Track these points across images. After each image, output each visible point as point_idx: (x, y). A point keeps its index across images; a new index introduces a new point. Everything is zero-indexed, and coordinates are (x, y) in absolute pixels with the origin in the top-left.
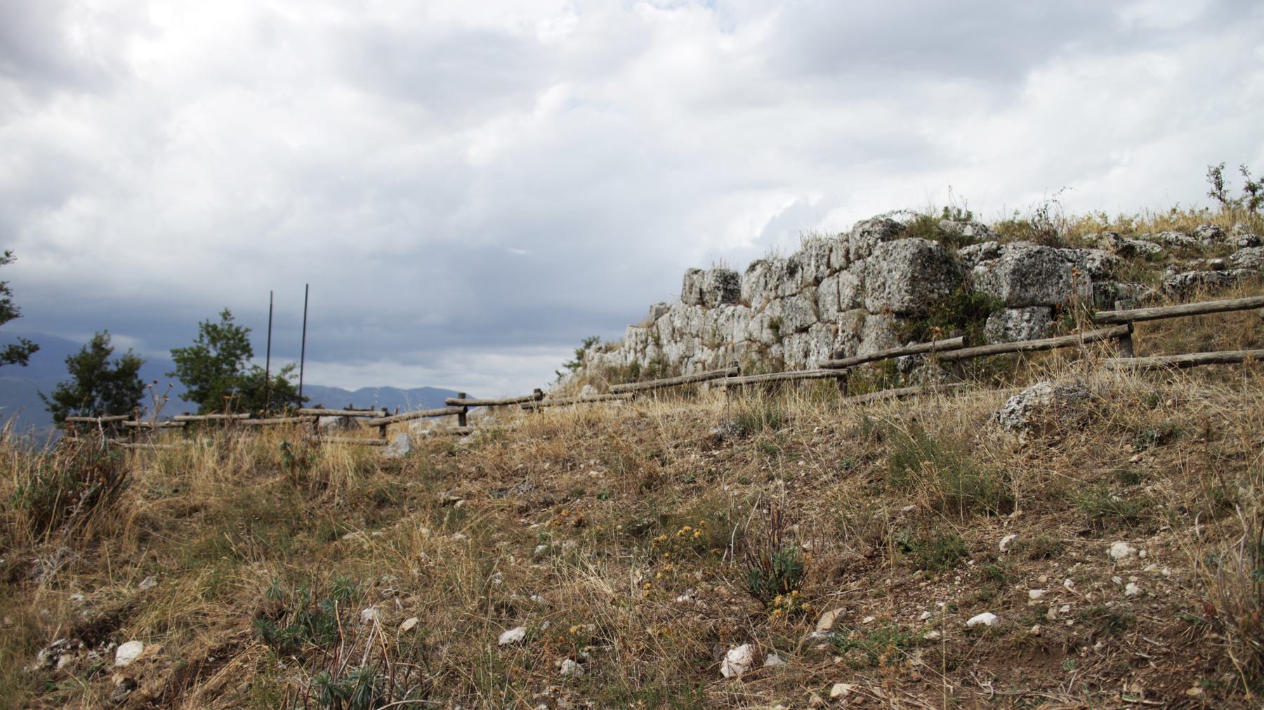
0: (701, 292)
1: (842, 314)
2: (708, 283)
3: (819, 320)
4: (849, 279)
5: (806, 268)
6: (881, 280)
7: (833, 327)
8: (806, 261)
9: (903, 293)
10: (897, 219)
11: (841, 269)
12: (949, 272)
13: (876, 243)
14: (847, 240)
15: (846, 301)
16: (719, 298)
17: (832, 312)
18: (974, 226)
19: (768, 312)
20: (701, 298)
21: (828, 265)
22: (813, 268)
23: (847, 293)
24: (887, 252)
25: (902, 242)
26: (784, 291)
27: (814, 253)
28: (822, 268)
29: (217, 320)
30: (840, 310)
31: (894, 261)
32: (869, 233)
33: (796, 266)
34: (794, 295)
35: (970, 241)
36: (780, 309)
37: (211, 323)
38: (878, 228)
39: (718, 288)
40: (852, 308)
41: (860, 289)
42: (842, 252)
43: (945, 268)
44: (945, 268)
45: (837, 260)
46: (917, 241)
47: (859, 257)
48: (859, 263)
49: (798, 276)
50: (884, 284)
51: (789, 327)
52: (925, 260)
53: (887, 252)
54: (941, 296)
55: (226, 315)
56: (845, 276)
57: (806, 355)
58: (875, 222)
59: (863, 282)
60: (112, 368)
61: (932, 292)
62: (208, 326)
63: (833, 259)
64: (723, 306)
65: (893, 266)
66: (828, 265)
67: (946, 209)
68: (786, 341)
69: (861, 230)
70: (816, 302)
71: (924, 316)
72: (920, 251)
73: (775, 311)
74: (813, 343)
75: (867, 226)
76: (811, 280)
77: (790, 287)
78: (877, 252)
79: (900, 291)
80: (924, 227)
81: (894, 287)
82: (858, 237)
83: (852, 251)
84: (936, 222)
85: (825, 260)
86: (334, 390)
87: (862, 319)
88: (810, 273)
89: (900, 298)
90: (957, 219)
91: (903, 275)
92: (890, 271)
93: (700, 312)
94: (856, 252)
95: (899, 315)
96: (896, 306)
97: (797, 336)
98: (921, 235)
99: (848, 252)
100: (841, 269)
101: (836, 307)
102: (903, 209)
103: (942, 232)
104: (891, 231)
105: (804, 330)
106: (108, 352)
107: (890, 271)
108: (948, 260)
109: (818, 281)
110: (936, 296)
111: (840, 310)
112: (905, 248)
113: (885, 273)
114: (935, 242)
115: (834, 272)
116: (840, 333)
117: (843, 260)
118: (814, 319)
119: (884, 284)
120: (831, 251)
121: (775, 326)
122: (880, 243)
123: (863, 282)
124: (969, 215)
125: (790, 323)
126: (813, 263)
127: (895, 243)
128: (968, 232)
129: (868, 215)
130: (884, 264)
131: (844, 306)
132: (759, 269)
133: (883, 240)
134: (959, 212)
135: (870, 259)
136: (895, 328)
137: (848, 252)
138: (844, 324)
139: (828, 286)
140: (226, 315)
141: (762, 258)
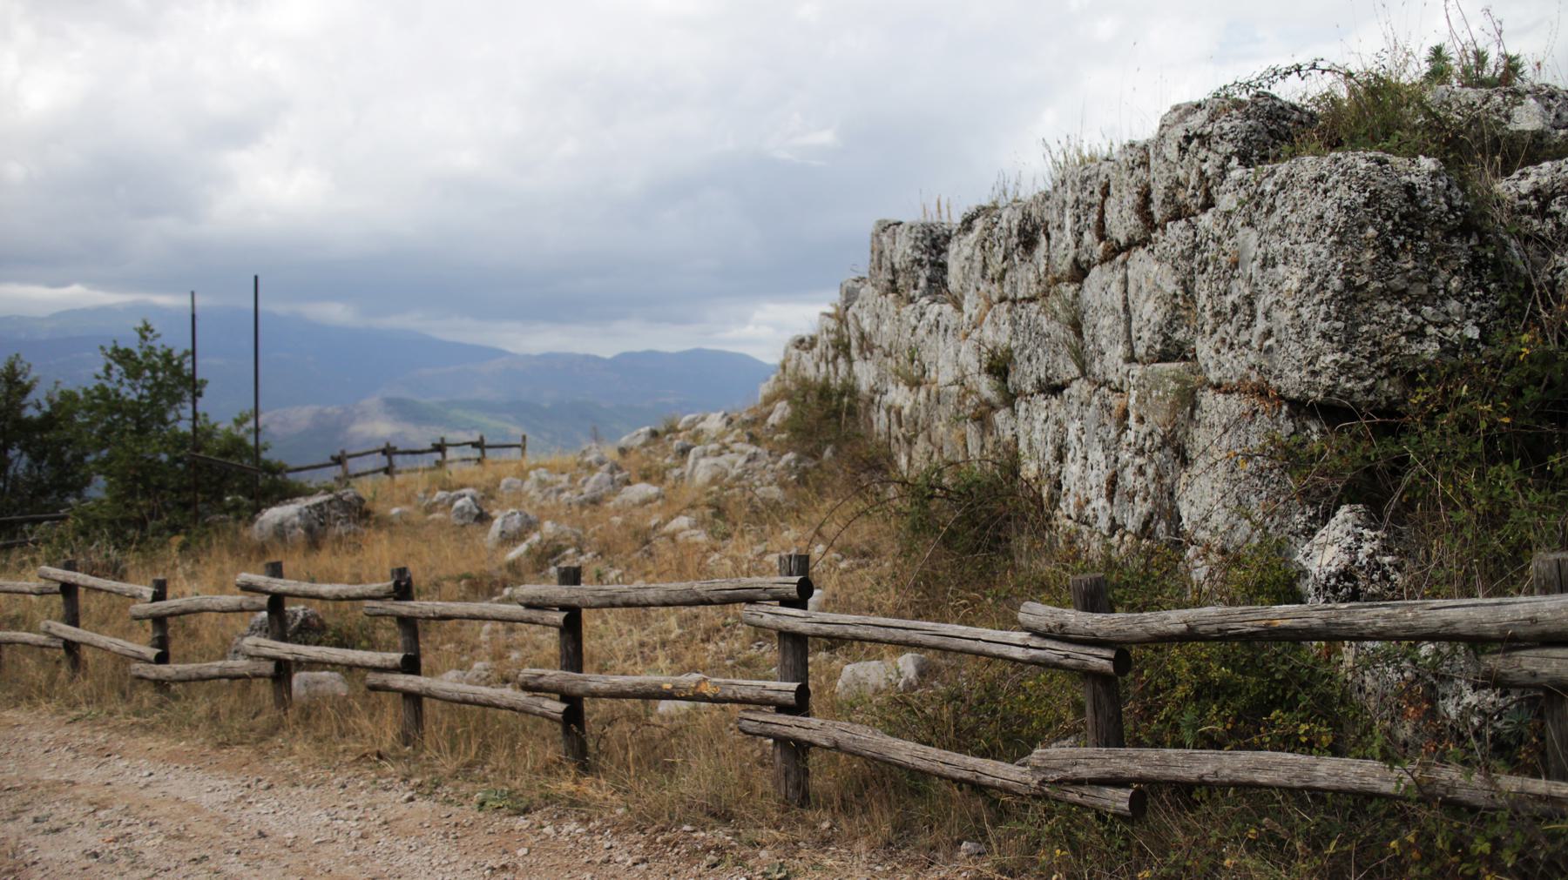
0: (894, 271)
1: (1137, 370)
2: (902, 250)
3: (1084, 374)
4: (1151, 273)
5: (1054, 234)
6: (1240, 289)
7: (1115, 401)
8: (1052, 216)
9: (1314, 341)
10: (1289, 91)
11: (1131, 245)
12: (1476, 265)
13: (1223, 170)
14: (1145, 164)
15: (1146, 338)
16: (922, 283)
17: (1112, 361)
18: (1547, 96)
19: (988, 333)
20: (893, 282)
21: (1102, 235)
22: (1069, 238)
23: (1149, 312)
24: (1256, 199)
25: (1308, 166)
26: (1014, 286)
27: (1070, 198)
28: (1088, 237)
29: (132, 343)
30: (1131, 359)
31: (1280, 230)
32: (1204, 139)
33: (1036, 228)
34: (1032, 299)
35: (1535, 149)
36: (1007, 328)
37: (121, 347)
38: (1233, 123)
39: (919, 262)
40: (1164, 357)
41: (1181, 307)
42: (1131, 199)
43: (1462, 250)
44: (1462, 250)
45: (1121, 223)
46: (1360, 161)
47: (1179, 213)
48: (1176, 229)
49: (1040, 251)
50: (1250, 301)
51: (1026, 375)
52: (1400, 222)
53: (1256, 199)
54: (1448, 349)
55: (145, 331)
56: (1142, 264)
57: (1060, 458)
58: (1223, 105)
59: (1187, 286)
60: (30, 413)
61: (1418, 334)
62: (116, 350)
63: (1111, 217)
64: (924, 301)
65: (1276, 246)
66: (1102, 235)
67: (1437, 53)
68: (1022, 406)
69: (1179, 132)
70: (1076, 327)
71: (1389, 420)
72: (1375, 198)
73: (997, 334)
74: (1073, 428)
75: (1196, 122)
76: (1065, 266)
77: (1025, 278)
78: (1226, 201)
79: (1303, 332)
80: (1373, 113)
81: (1284, 317)
82: (1172, 152)
83: (1158, 195)
84: (1414, 96)
85: (1094, 217)
86: (587, 357)
87: (1188, 399)
88: (1060, 248)
89: (1306, 361)
90: (1472, 79)
91: (1315, 280)
92: (1267, 263)
93: (892, 308)
94: (1170, 198)
95: (1300, 408)
96: (1292, 381)
97: (1040, 400)
98: (1372, 140)
99: (1146, 196)
100: (1131, 245)
101: (1121, 350)
102: (1304, 59)
103: (1436, 124)
104: (1270, 129)
105: (1054, 389)
106: (26, 390)
107: (1267, 263)
108: (1470, 223)
109: (1080, 272)
110: (1431, 349)
111: (1131, 359)
112: (1319, 186)
113: (1253, 268)
114: (1427, 164)
115: (1115, 252)
116: (1132, 421)
117: (1134, 220)
118: (1074, 370)
119: (1250, 301)
120: (1106, 192)
121: (999, 367)
122: (1237, 173)
123: (1187, 286)
124: (1512, 67)
125: (1026, 367)
126: (1068, 222)
127: (1283, 168)
128: (1528, 118)
129: (1198, 87)
130: (1248, 238)
131: (1140, 350)
132: (979, 224)
133: (1245, 160)
134: (1481, 58)
135: (1206, 220)
136: (1291, 457)
137: (1146, 196)
138: (1141, 400)
139: (1101, 287)
140: (145, 331)
141: (986, 202)
